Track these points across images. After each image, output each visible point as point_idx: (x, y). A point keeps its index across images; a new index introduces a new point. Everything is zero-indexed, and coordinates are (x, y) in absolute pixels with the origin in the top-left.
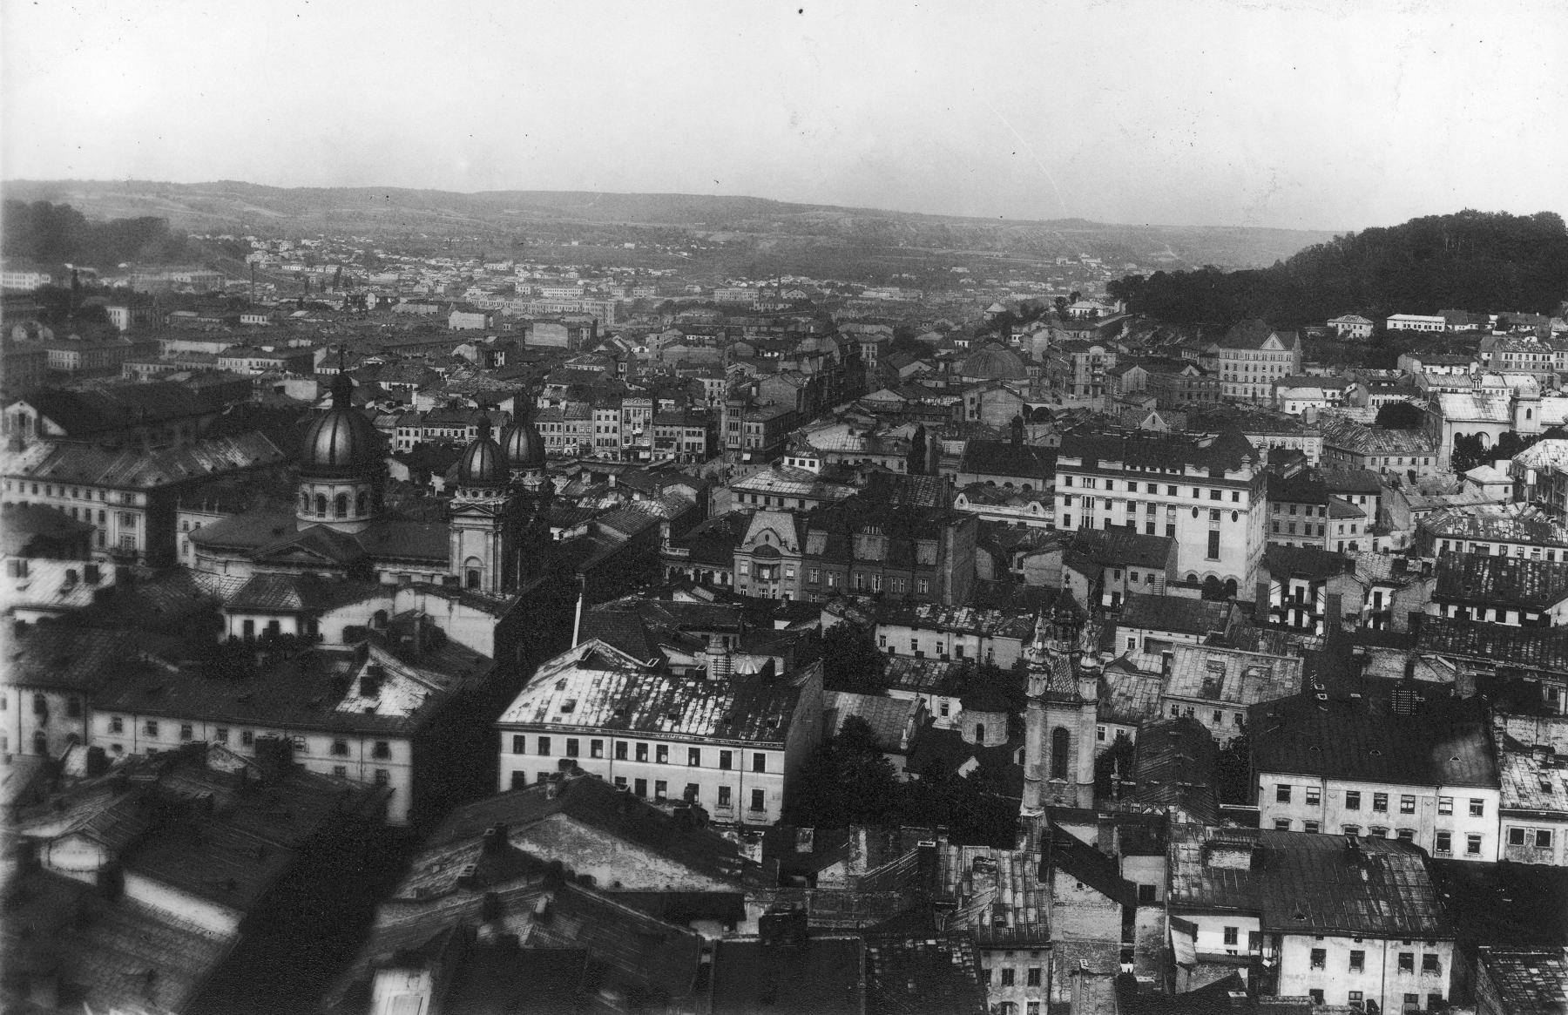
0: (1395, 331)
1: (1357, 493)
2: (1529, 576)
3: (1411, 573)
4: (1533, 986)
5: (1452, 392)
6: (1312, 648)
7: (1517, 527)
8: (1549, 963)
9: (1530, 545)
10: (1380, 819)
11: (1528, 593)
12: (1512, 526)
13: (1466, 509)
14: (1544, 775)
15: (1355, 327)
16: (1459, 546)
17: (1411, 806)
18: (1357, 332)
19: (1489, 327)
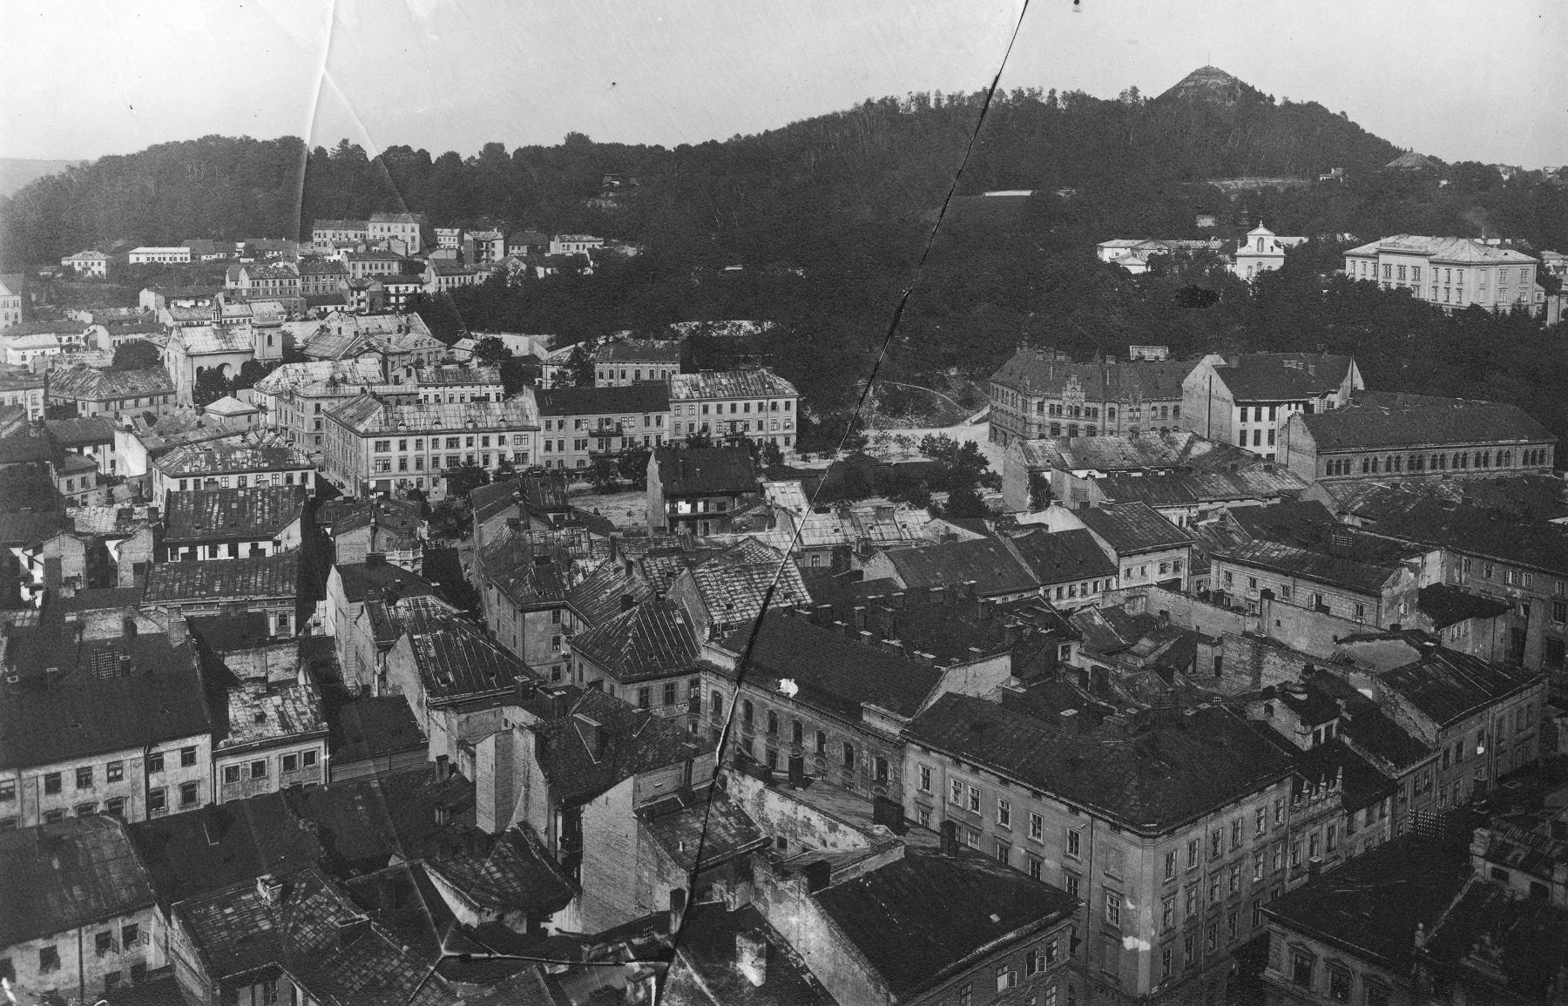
0: (138, 265)
1: (88, 443)
2: (259, 504)
3: (138, 522)
4: (227, 927)
5: (198, 325)
6: (27, 623)
7: (254, 456)
8: (243, 898)
9: (234, 473)
10: (85, 796)
11: (259, 521)
12: (249, 455)
13: (204, 444)
14: (257, 706)
15: (93, 264)
16: (197, 483)
17: (119, 772)
18: (96, 269)
19: (237, 255)
